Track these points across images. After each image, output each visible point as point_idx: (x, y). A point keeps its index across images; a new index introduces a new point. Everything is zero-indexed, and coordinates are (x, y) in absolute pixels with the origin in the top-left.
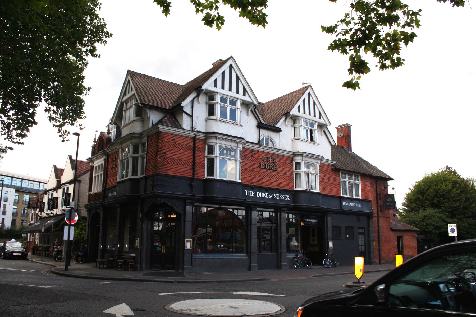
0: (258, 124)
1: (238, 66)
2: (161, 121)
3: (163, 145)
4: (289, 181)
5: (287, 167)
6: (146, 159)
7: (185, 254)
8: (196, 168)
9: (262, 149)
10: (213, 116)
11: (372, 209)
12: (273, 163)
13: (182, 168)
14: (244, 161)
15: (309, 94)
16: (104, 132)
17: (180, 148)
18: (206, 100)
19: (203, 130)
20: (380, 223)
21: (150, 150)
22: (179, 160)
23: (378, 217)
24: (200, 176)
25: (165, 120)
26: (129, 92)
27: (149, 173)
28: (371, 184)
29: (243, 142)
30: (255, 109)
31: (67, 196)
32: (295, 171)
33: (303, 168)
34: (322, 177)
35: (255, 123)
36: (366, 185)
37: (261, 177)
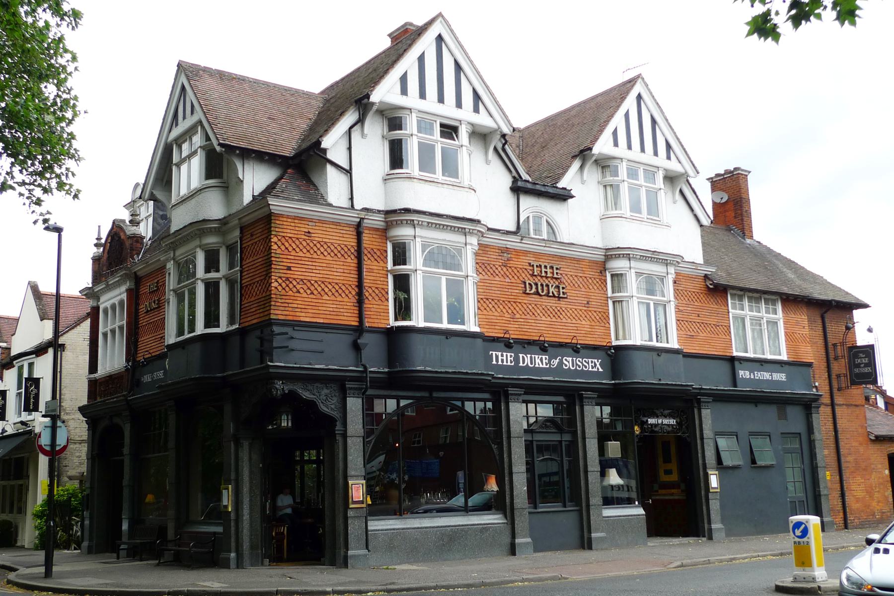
0: (513, 182)
1: (456, 39)
2: (274, 188)
3: (283, 248)
4: (598, 324)
5: (591, 287)
6: (241, 284)
7: (349, 522)
8: (366, 301)
9: (527, 245)
10: (401, 168)
11: (817, 384)
12: (556, 279)
13: (331, 302)
14: (483, 277)
15: (639, 97)
16: (123, 221)
17: (326, 253)
18: (383, 130)
19: (379, 205)
20: (840, 423)
21: (248, 261)
22: (323, 282)
23: (833, 405)
24: (376, 321)
25: (282, 184)
26: (184, 118)
27: (249, 319)
28: (810, 321)
29: (478, 231)
30: (504, 145)
31: (31, 386)
32: (611, 298)
33: (632, 284)
34: (680, 308)
35: (506, 181)
36: (797, 323)
37: (528, 316)
